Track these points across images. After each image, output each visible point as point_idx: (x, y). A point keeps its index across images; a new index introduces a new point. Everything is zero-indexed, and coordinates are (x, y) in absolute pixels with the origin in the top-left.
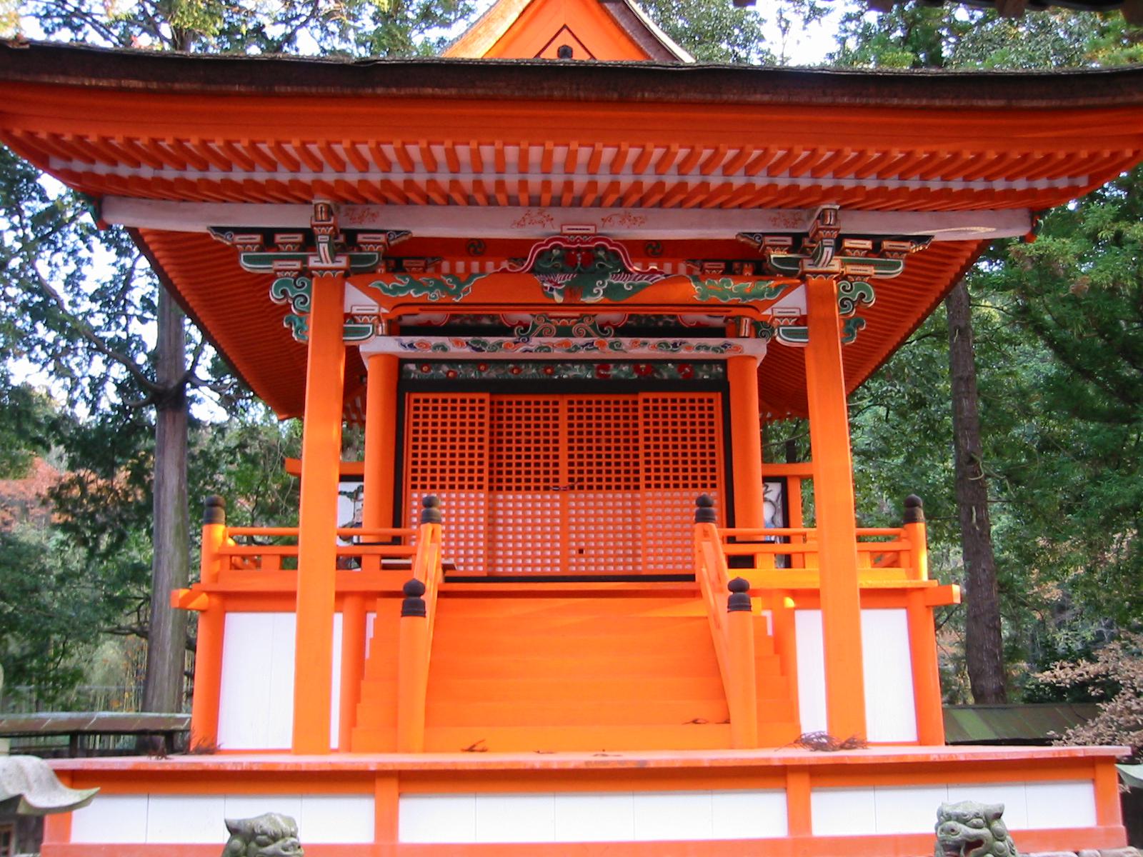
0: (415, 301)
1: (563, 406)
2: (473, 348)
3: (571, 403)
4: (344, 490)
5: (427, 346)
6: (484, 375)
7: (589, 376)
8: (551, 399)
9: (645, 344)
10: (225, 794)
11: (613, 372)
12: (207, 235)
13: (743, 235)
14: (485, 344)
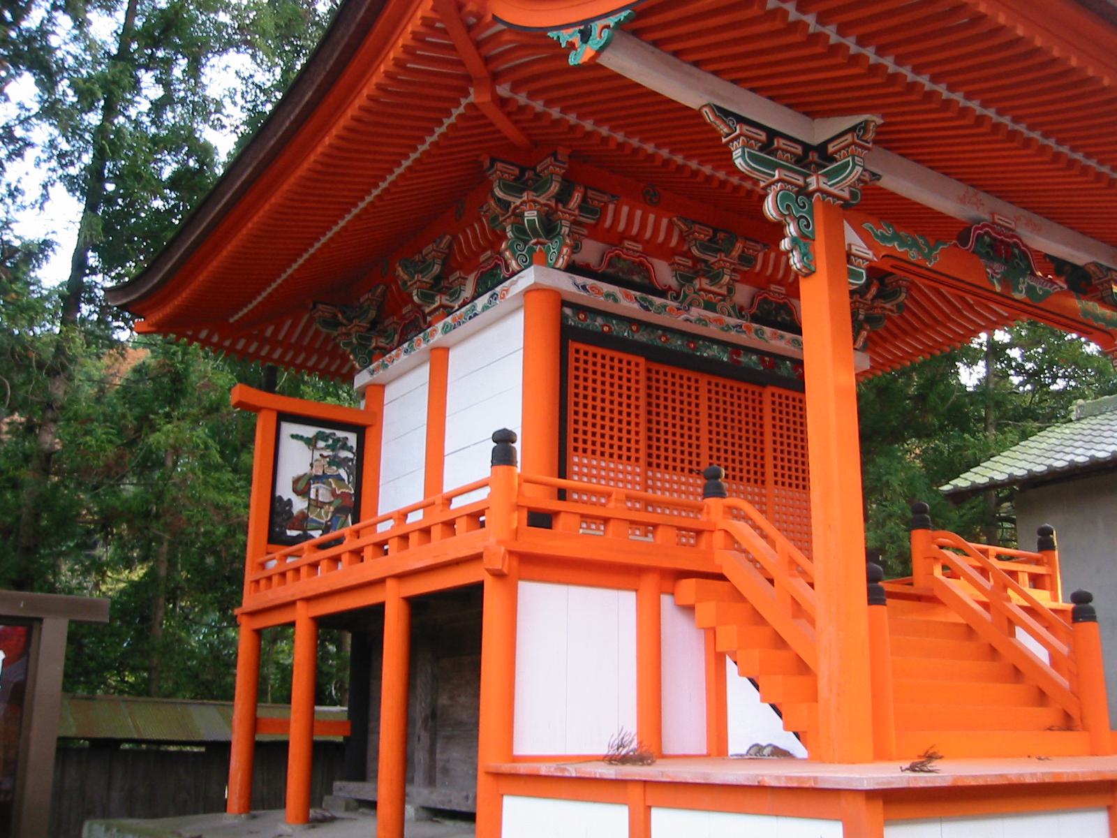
0: (896, 255)
1: (703, 385)
2: (641, 305)
3: (709, 383)
4: (300, 433)
5: (599, 292)
6: (636, 337)
7: (725, 359)
8: (693, 376)
9: (782, 337)
10: (941, 818)
11: (743, 359)
12: (698, 114)
13: (1095, 264)
14: (651, 303)
